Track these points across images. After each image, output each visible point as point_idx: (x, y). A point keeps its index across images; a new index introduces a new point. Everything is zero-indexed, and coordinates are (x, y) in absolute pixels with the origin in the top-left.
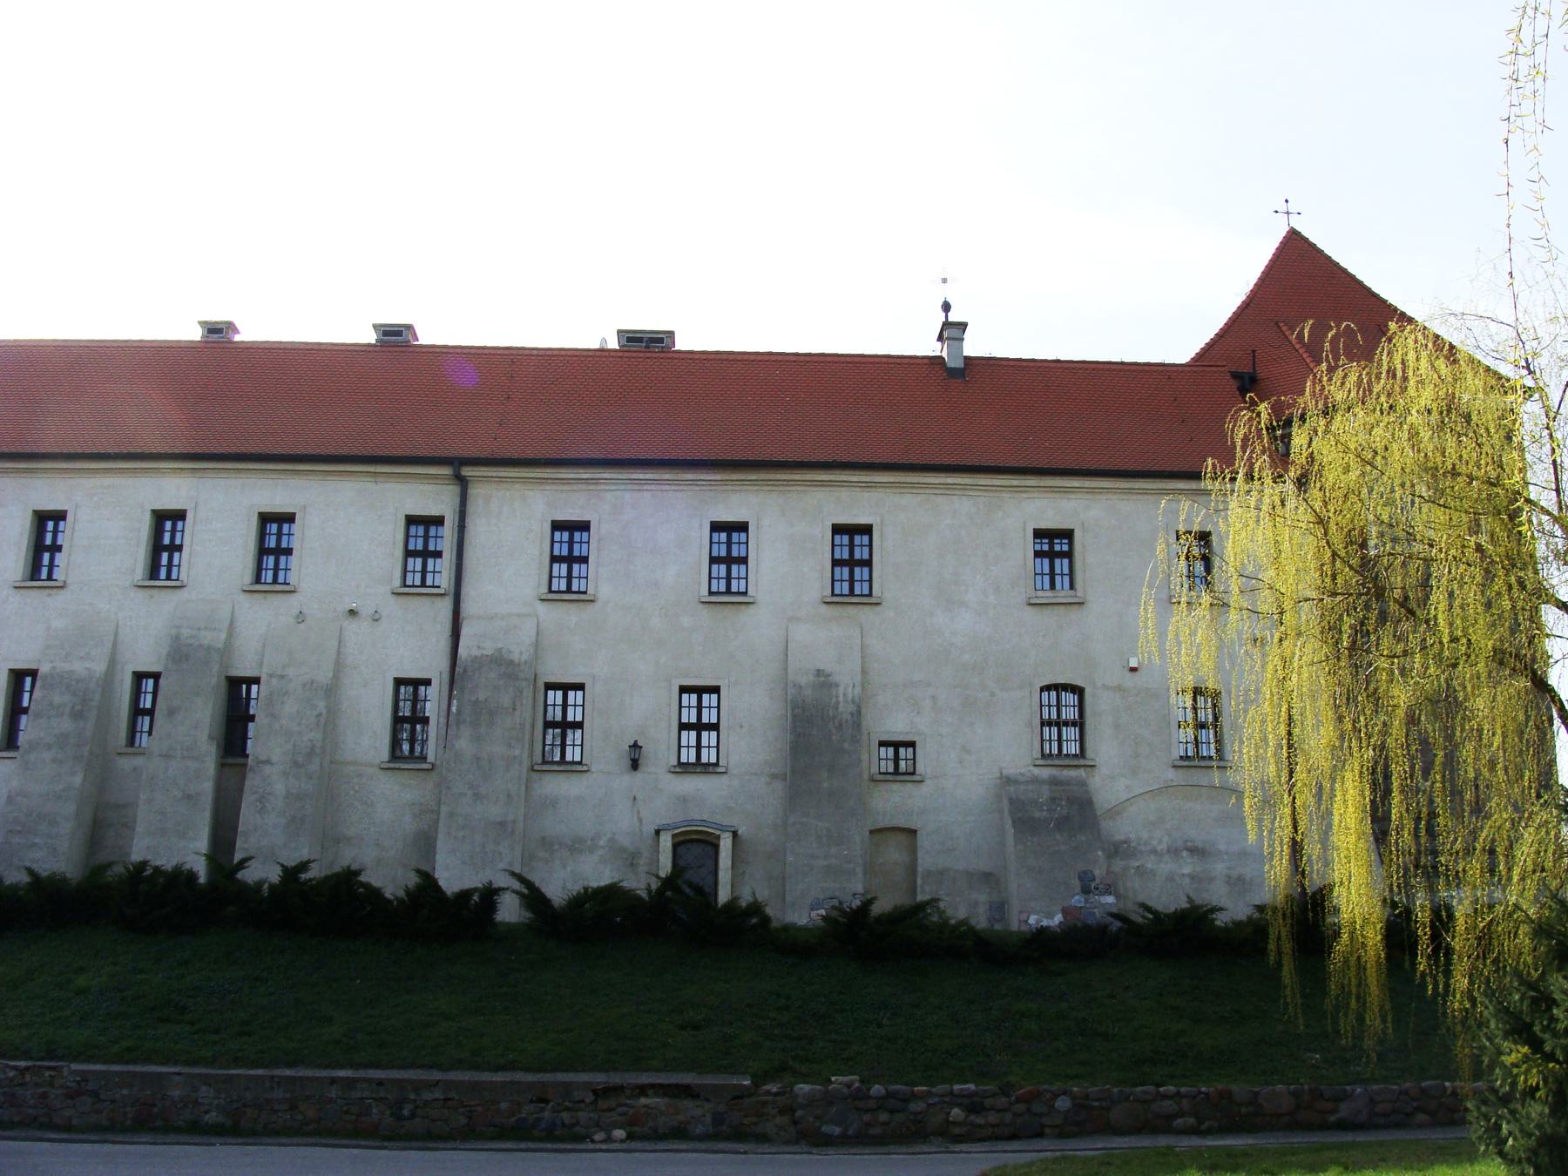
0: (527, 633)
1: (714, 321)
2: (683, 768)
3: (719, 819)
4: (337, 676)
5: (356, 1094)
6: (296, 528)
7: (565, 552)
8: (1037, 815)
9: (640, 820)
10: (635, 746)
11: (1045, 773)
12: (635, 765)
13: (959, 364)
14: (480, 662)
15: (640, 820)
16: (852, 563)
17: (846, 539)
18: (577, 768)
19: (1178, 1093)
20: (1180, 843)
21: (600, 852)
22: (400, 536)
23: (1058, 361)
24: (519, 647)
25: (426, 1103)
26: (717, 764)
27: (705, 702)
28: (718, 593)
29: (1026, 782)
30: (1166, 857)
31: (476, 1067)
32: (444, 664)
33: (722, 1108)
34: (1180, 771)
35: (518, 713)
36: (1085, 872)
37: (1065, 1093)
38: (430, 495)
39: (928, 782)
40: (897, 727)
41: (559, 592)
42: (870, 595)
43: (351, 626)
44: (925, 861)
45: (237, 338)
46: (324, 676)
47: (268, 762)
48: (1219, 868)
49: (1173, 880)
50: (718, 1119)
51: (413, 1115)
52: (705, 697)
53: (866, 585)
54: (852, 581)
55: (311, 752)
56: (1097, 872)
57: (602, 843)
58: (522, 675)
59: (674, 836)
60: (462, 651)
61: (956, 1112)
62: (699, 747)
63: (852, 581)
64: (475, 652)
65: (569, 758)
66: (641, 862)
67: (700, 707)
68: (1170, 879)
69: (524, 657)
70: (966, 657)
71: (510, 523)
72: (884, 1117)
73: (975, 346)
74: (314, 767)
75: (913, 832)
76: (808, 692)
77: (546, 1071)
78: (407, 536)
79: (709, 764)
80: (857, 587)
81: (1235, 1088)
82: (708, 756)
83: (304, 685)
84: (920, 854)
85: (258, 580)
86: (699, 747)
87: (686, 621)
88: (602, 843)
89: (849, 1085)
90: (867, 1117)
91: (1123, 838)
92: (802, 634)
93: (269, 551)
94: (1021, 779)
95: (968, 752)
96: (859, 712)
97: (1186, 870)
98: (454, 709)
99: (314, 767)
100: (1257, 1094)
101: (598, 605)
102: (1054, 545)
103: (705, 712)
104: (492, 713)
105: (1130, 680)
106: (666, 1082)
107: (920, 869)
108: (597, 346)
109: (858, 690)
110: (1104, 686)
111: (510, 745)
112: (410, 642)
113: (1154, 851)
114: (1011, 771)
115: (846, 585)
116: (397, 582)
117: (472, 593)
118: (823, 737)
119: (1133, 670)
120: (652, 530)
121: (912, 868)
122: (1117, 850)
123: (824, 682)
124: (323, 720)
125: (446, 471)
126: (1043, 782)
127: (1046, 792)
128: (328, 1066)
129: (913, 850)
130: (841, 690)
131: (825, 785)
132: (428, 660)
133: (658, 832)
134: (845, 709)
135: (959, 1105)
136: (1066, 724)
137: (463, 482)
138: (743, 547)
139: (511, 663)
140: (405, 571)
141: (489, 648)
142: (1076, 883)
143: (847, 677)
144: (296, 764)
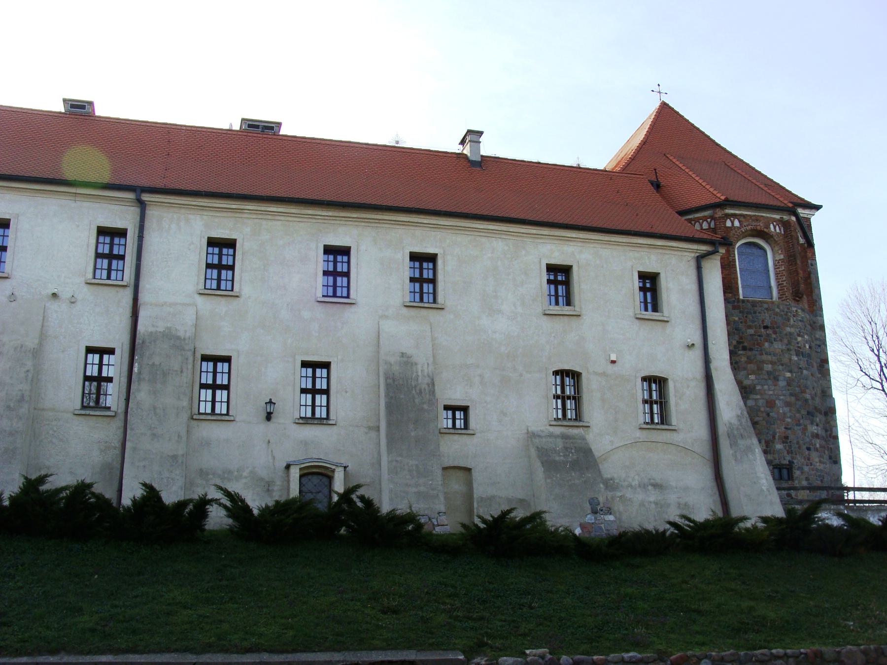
0: (189, 317)
1: (303, 120)
2: (305, 421)
3: (333, 458)
4: (41, 344)
6: (11, 232)
7: (107, 251)
8: (557, 458)
9: (274, 458)
11: (558, 431)
12: (269, 416)
14: (154, 337)
15: (274, 458)
16: (220, 267)
17: (108, 240)
18: (226, 418)
19: (786, 654)
20: (646, 481)
21: (244, 481)
22: (94, 241)
23: (539, 163)
24: (184, 325)
26: (328, 418)
27: (219, 369)
29: (546, 436)
30: (638, 489)
31: (225, 650)
32: (126, 338)
34: (644, 432)
35: (184, 374)
36: (592, 499)
37: (706, 657)
38: (118, 213)
39: (478, 435)
40: (457, 397)
41: (342, 297)
42: (348, 297)
43: (53, 306)
44: (479, 491)
46: (31, 342)
48: (672, 498)
49: (644, 506)
52: (219, 365)
53: (345, 290)
54: (219, 280)
55: (22, 399)
56: (601, 499)
57: (245, 474)
58: (187, 348)
59: (301, 469)
60: (140, 328)
62: (214, 402)
63: (219, 280)
64: (151, 329)
65: (217, 411)
66: (276, 488)
67: (215, 373)
68: (642, 504)
69: (188, 335)
70: (503, 348)
71: (177, 239)
73: (489, 148)
74: (24, 410)
75: (468, 470)
76: (396, 368)
77: (287, 652)
79: (321, 419)
80: (223, 284)
81: (824, 649)
82: (320, 413)
83: (15, 349)
84: (475, 486)
86: (214, 402)
87: (306, 314)
88: (245, 474)
89: (542, 657)
91: (609, 476)
92: (389, 327)
94: (543, 434)
95: (505, 415)
96: (433, 384)
97: (652, 499)
98: (136, 370)
99: (24, 410)
100: (839, 652)
101: (242, 300)
102: (560, 276)
103: (219, 376)
104: (165, 374)
106: (394, 659)
107: (475, 496)
108: (228, 128)
109: (431, 368)
110: (595, 373)
111: (179, 399)
112: (101, 319)
113: (631, 486)
114: (533, 428)
115: (105, 273)
116: (90, 275)
117: (148, 286)
118: (409, 403)
119: (613, 362)
120: (282, 250)
121: (469, 496)
122: (610, 484)
123: (407, 360)
124: (30, 376)
125: (131, 196)
126: (556, 437)
127: (560, 444)
128: (89, 653)
129: (469, 484)
130: (419, 368)
131: (413, 434)
133: (288, 467)
134: (423, 382)
136: (569, 398)
137: (142, 205)
138: (122, 248)
139: (178, 338)
141: (161, 327)
142: (588, 507)
143: (422, 358)
144: (9, 407)
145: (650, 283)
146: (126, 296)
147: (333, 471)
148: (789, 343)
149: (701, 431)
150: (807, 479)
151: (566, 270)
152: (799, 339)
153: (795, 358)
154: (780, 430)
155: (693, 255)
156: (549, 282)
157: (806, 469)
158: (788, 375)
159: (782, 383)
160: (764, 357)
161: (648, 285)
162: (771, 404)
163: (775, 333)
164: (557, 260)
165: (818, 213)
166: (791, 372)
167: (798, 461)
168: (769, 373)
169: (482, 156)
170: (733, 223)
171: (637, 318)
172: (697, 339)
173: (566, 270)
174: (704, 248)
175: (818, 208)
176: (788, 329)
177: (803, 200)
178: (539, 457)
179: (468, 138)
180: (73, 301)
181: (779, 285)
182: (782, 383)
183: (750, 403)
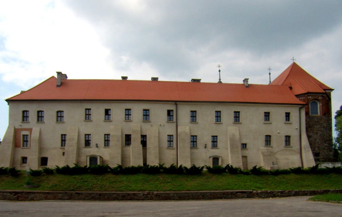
5: (197, 194)
10: (206, 145)
11: (266, 148)
12: (97, 144)
13: (248, 85)
25: (208, 195)
28: (145, 120)
33: (248, 194)
38: (172, 107)
45: (67, 79)
47: (150, 148)
50: (248, 196)
51: (206, 197)
59: (90, 157)
61: (279, 194)
72: (270, 194)
73: (250, 82)
78: (125, 112)
85: (86, 119)
90: (268, 195)
93: (87, 115)
105: (278, 135)
119: (279, 133)
125: (174, 103)
127: (266, 151)
132: (173, 133)
135: (280, 193)
137: (176, 104)
140: (125, 118)
142: (272, 164)
145: (288, 115)
146: (175, 125)
147: (219, 158)
148: (321, 125)
149: (298, 147)
150: (323, 156)
151: (269, 113)
152: (324, 124)
153: (322, 129)
154: (317, 145)
155: (299, 108)
156: (265, 116)
157: (323, 154)
158: (320, 133)
159: (319, 135)
160: (315, 129)
161: (287, 115)
162: (315, 139)
163: (318, 123)
164: (266, 111)
165: (333, 91)
166: (321, 132)
167: (321, 152)
168: (316, 133)
169: (249, 85)
170: (309, 97)
171: (285, 123)
172: (298, 127)
173: (269, 113)
174: (301, 106)
175: (333, 90)
176: (321, 122)
177: (329, 88)
178: (262, 154)
179: (245, 80)
180: (164, 126)
181: (320, 111)
182: (319, 135)
183: (311, 139)
